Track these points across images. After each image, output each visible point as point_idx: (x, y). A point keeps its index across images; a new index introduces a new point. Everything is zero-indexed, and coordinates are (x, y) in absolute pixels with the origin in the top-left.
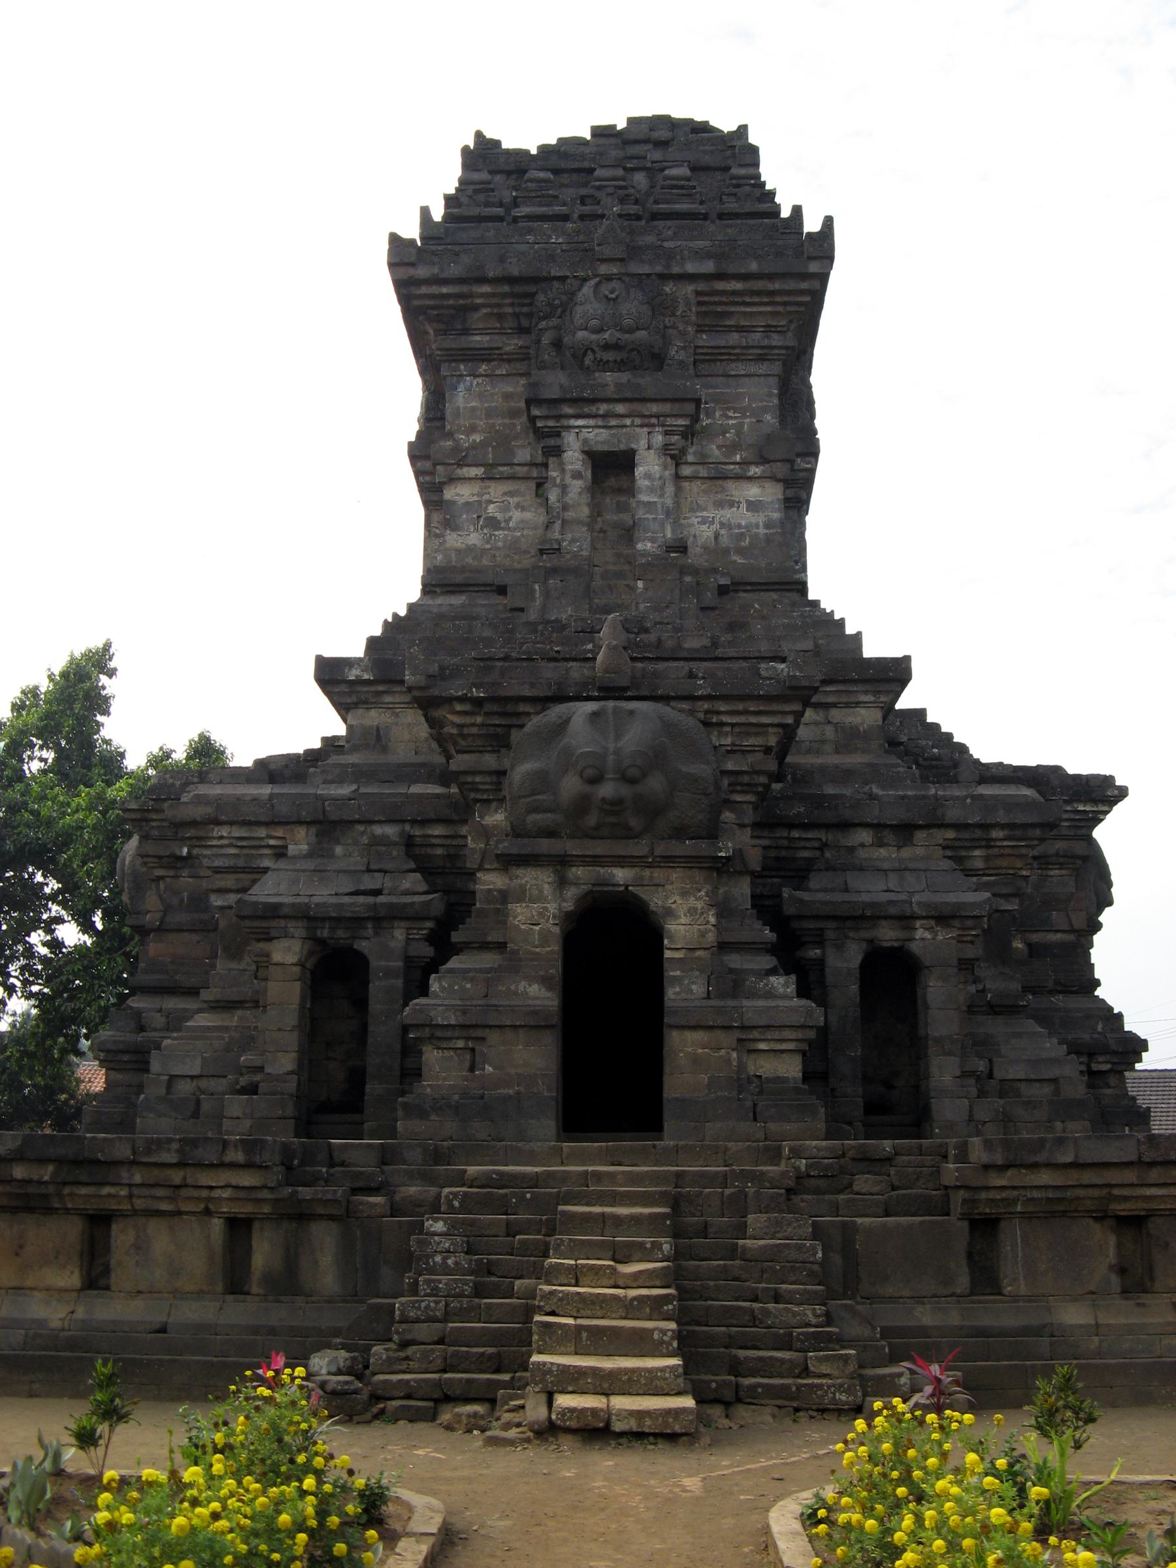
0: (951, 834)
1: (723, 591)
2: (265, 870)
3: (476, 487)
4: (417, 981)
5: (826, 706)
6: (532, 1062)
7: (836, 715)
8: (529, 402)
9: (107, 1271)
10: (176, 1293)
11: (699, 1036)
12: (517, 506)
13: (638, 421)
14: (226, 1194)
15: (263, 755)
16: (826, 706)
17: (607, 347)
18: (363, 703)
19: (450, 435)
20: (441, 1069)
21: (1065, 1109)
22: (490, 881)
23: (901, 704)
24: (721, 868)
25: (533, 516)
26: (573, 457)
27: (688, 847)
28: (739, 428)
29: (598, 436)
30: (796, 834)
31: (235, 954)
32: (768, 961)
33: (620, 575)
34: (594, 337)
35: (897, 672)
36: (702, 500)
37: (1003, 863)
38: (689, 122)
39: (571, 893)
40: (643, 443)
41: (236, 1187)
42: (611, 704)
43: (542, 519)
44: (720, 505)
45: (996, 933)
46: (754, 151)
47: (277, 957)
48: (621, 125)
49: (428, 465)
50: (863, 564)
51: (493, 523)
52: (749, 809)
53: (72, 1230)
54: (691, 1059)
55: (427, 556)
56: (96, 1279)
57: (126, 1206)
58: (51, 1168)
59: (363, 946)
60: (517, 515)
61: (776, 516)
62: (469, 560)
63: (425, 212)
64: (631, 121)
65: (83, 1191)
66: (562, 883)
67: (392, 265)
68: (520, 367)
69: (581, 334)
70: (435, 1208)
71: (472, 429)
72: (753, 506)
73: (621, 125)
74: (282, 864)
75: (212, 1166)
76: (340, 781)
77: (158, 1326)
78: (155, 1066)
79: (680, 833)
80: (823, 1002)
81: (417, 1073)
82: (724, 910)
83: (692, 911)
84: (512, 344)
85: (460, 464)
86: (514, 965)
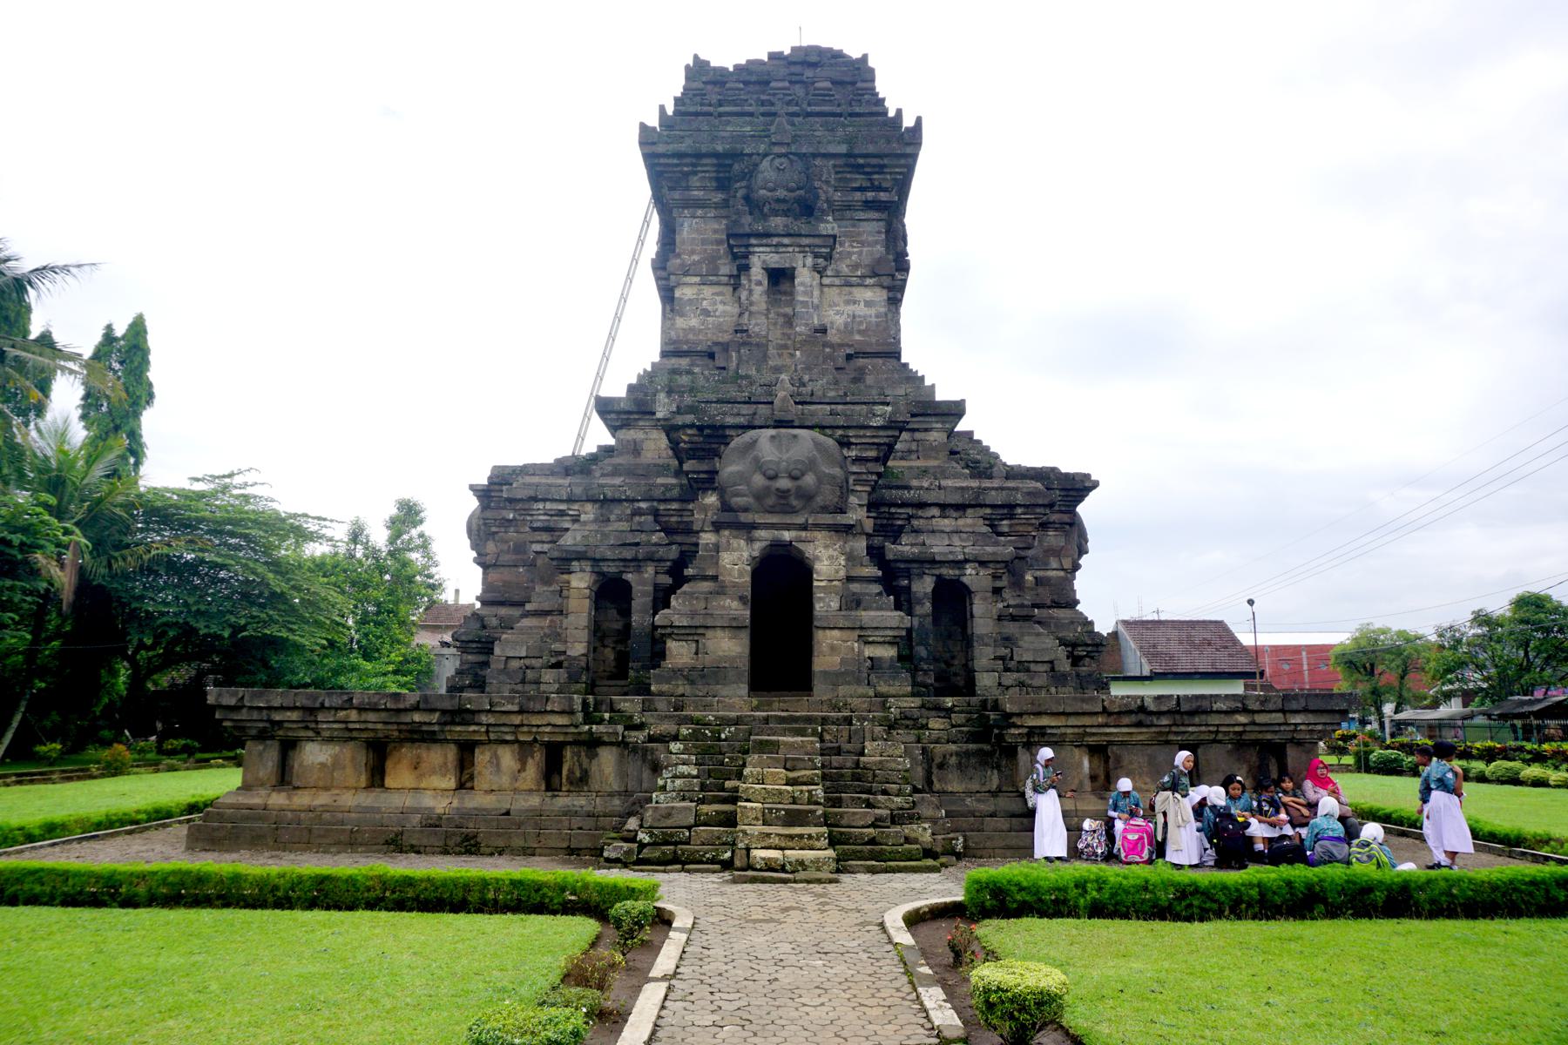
0: (988, 511)
1: (849, 357)
2: (567, 530)
3: (695, 290)
4: (662, 599)
5: (913, 430)
6: (730, 647)
7: (918, 435)
8: (729, 236)
9: (472, 778)
10: (515, 790)
11: (836, 633)
14: (548, 729)
15: (560, 456)
16: (913, 430)
17: (778, 201)
18: (626, 425)
19: (679, 256)
20: (679, 653)
21: (1058, 678)
22: (707, 538)
23: (959, 428)
24: (847, 530)
25: (733, 309)
26: (757, 272)
27: (827, 519)
28: (860, 254)
29: (774, 260)
30: (893, 510)
31: (548, 583)
32: (876, 588)
33: (785, 347)
35: (955, 410)
36: (836, 299)
37: (1020, 528)
38: (830, 50)
39: (758, 546)
40: (800, 263)
41: (554, 726)
42: (783, 431)
43: (736, 310)
44: (847, 302)
45: (1012, 568)
46: (872, 71)
47: (574, 584)
48: (787, 52)
49: (664, 274)
50: (937, 345)
51: (706, 313)
52: (865, 496)
53: (451, 753)
54: (831, 648)
55: (663, 332)
56: (465, 783)
57: (484, 738)
58: (437, 715)
59: (629, 577)
60: (721, 308)
61: (883, 310)
62: (691, 336)
63: (662, 109)
64: (793, 49)
65: (458, 728)
66: (751, 540)
67: (642, 144)
68: (723, 212)
69: (762, 192)
70: (676, 738)
71: (693, 252)
72: (868, 304)
73: (787, 52)
74: (576, 526)
75: (539, 712)
76: (613, 474)
78: (497, 651)
79: (825, 509)
80: (910, 613)
81: (662, 655)
82: (851, 558)
83: (831, 557)
84: (718, 197)
85: (686, 274)
86: (721, 591)
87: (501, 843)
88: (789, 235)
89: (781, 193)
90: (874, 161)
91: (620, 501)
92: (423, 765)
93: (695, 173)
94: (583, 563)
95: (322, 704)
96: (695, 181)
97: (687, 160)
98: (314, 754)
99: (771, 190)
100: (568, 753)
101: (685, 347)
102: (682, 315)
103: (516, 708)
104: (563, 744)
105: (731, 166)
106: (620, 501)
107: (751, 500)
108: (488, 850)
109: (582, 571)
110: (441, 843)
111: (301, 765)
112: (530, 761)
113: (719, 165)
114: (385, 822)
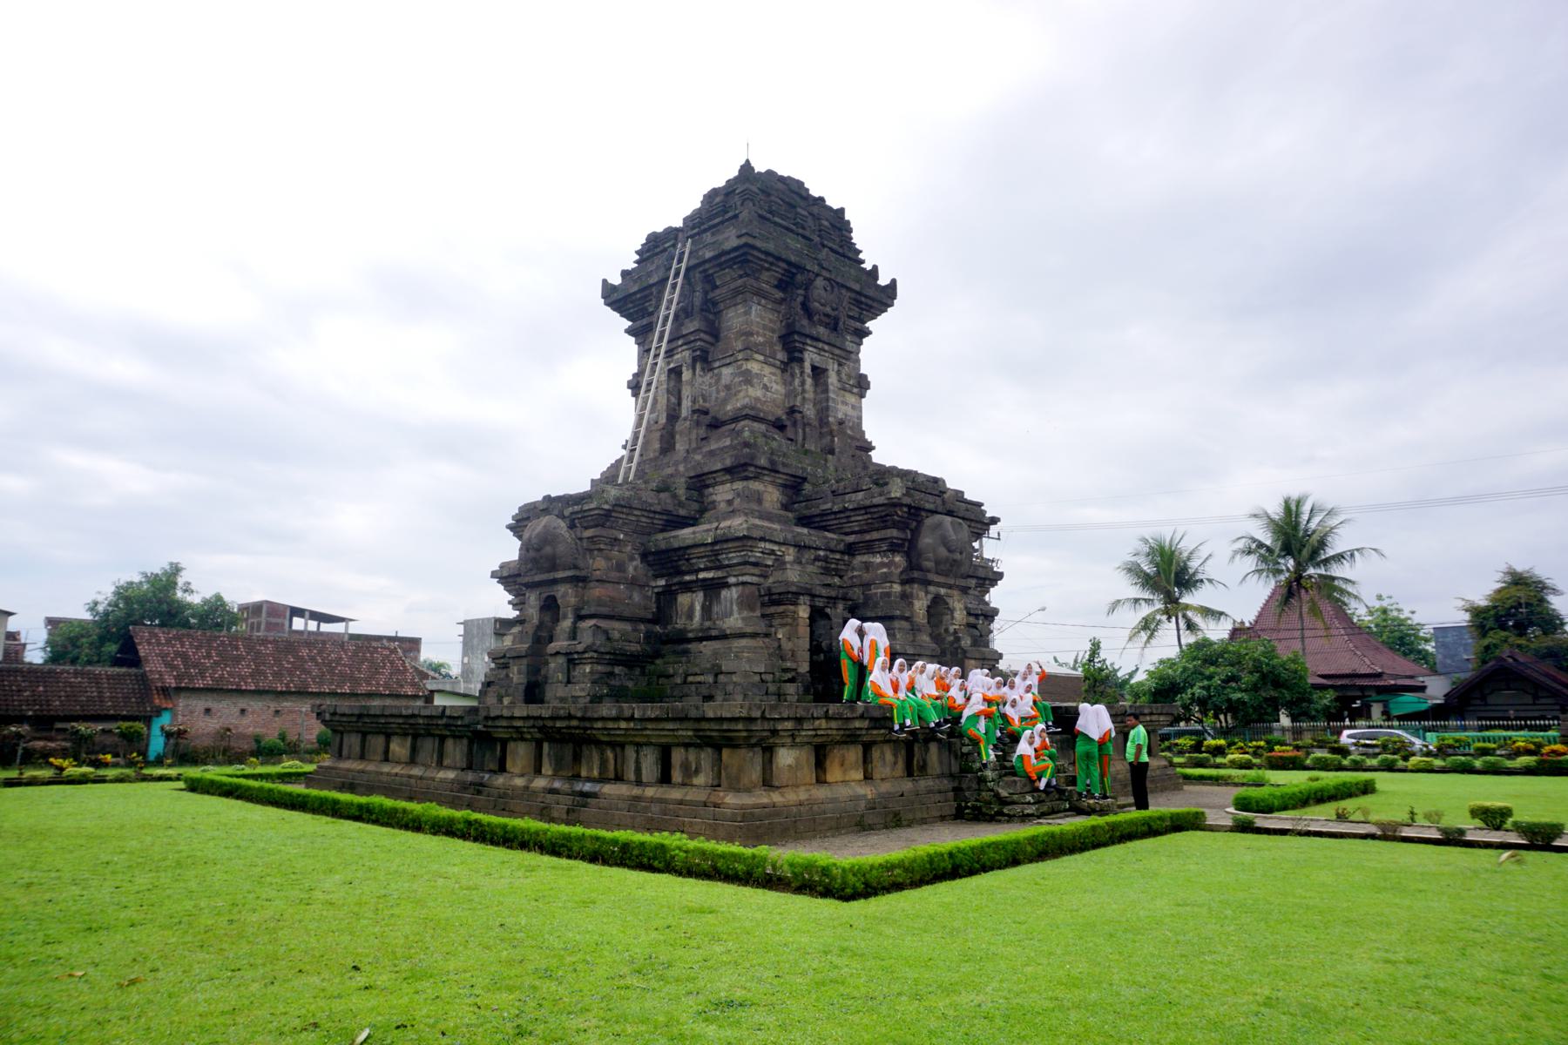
29: (817, 358)
51: (765, 387)
56: (868, 777)
60: (775, 386)
66: (927, 593)
84: (779, 295)
87: (910, 816)
89: (828, 310)
91: (810, 548)
93: (768, 270)
96: (765, 276)
98: (786, 757)
106: (810, 548)
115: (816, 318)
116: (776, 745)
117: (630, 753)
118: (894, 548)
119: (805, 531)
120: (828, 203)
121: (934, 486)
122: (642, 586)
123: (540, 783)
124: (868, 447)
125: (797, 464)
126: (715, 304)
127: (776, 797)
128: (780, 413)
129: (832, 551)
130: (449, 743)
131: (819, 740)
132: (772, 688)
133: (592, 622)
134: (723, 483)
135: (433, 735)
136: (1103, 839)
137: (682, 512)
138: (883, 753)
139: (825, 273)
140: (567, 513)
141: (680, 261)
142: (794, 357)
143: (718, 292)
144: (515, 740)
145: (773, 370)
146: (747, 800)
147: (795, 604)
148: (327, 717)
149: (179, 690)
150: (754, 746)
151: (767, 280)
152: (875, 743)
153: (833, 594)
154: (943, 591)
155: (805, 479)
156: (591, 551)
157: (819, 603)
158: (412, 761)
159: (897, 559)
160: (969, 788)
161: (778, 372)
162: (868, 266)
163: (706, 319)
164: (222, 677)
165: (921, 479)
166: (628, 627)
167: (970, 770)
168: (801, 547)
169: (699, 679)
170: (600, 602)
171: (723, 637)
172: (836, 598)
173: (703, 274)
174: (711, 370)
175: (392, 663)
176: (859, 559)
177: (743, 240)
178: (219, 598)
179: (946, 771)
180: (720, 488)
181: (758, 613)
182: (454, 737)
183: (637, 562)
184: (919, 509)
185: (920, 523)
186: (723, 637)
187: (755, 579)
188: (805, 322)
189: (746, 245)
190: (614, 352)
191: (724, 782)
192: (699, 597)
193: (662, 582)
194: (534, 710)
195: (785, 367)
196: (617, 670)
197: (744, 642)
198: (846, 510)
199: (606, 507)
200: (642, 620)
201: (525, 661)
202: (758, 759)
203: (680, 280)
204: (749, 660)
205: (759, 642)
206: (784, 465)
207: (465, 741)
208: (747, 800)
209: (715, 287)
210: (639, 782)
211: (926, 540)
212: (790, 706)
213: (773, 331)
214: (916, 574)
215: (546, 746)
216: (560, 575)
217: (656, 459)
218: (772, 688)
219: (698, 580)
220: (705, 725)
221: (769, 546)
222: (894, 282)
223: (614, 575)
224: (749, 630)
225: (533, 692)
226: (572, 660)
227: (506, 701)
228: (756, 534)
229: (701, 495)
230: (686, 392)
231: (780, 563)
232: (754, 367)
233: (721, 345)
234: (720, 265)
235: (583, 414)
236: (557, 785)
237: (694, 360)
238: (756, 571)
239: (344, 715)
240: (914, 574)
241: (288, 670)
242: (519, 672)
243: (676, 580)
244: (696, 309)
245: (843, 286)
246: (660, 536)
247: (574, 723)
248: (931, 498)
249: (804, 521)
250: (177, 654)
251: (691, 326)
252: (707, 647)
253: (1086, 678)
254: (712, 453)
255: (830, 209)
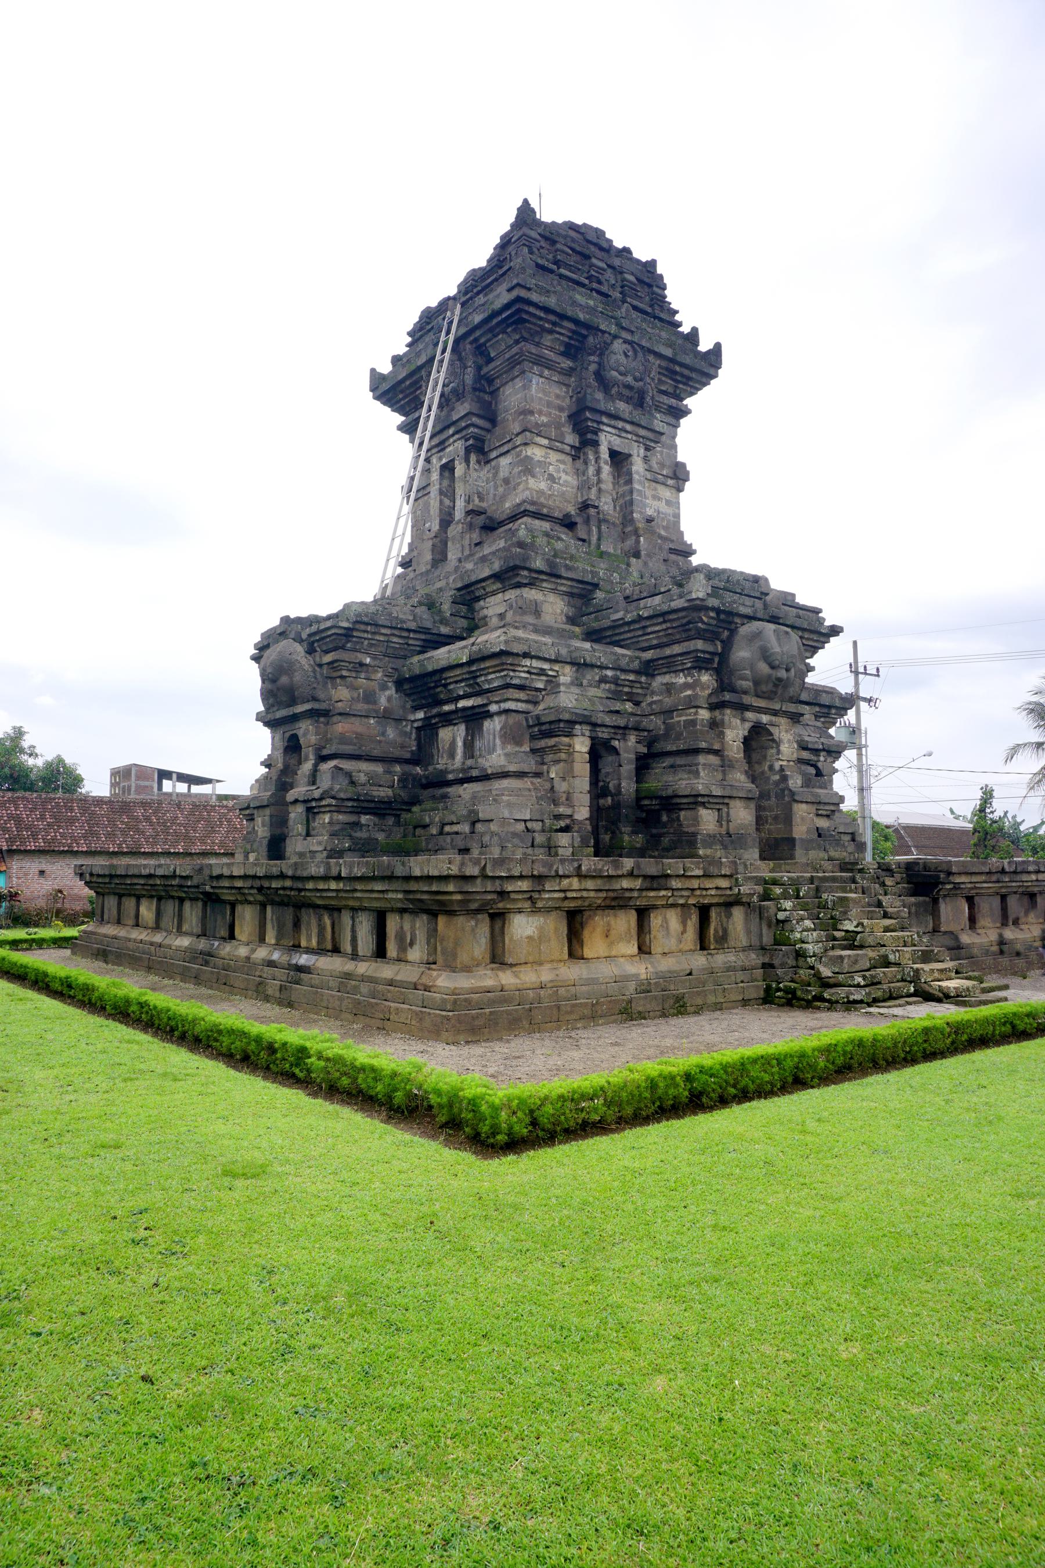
12: (564, 471)
13: (634, 438)
29: (618, 444)
34: (620, 377)
47: (578, 748)
51: (551, 478)
53: (633, 916)
56: (644, 950)
58: (640, 880)
60: (564, 477)
66: (743, 720)
77: (688, 972)
84: (567, 363)
87: (700, 1001)
88: (632, 423)
89: (629, 379)
90: (686, 372)
91: (593, 666)
92: (613, 932)
93: (551, 332)
94: (585, 727)
95: (557, 871)
96: (547, 340)
97: (552, 318)
98: (523, 927)
99: (621, 374)
100: (713, 913)
101: (545, 511)
102: (533, 476)
103: (700, 873)
104: (711, 905)
105: (585, 337)
106: (593, 666)
107: (751, 684)
108: (692, 1009)
109: (583, 735)
110: (660, 1008)
111: (511, 940)
112: (689, 923)
113: (573, 332)
114: (610, 993)
115: (614, 391)
116: (509, 911)
117: (346, 918)
118: (701, 664)
119: (587, 645)
120: (636, 255)
121: (756, 586)
122: (398, 720)
123: (261, 953)
124: (687, 552)
125: (583, 568)
126: (490, 381)
127: (507, 978)
128: (572, 510)
129: (623, 671)
130: (187, 905)
131: (572, 904)
132: (539, 839)
133: (332, 763)
134: (494, 593)
135: (173, 897)
136: (940, 1045)
137: (444, 630)
138: (665, 920)
139: (625, 335)
140: (304, 636)
141: (448, 333)
142: (586, 440)
143: (492, 365)
144: (241, 903)
145: (562, 457)
146: (464, 982)
147: (570, 735)
148: (88, 878)
149: (11, 852)
150: (478, 911)
151: (549, 346)
152: (655, 907)
153: (622, 722)
154: (765, 719)
155: (596, 586)
156: (333, 678)
157: (603, 734)
158: (157, 927)
159: (705, 678)
160: (783, 965)
161: (569, 459)
162: (685, 329)
163: (480, 400)
164: (54, 839)
165: (736, 578)
166: (378, 768)
167: (787, 942)
168: (580, 665)
169: (455, 828)
170: (343, 739)
171: (485, 777)
172: (625, 728)
173: (474, 344)
174: (488, 462)
175: (229, 821)
176: (660, 680)
177: (515, 293)
178: (60, 760)
179: (755, 941)
180: (491, 600)
181: (526, 748)
182: (191, 899)
183: (391, 691)
184: (730, 614)
185: (733, 632)
186: (485, 777)
187: (521, 706)
188: (599, 396)
189: (519, 299)
190: (387, 454)
191: (440, 959)
192: (461, 730)
193: (420, 715)
194: (276, 867)
195: (577, 453)
196: (364, 819)
197: (505, 783)
198: (640, 618)
199: (345, 624)
200: (398, 760)
201: (267, 811)
202: (483, 929)
203: (447, 355)
204: (509, 805)
205: (527, 783)
206: (568, 568)
207: (200, 904)
208: (464, 982)
209: (490, 360)
210: (355, 956)
211: (741, 653)
212: (562, 861)
213: (561, 409)
214: (727, 696)
215: (269, 909)
216: (300, 709)
217: (428, 572)
218: (539, 839)
219: (456, 711)
220: (413, 886)
221: (536, 663)
222: (718, 347)
223: (361, 707)
224: (512, 768)
225: (276, 847)
226: (311, 812)
227: (252, 857)
228: (517, 648)
229: (471, 610)
230: (460, 490)
231: (553, 684)
232: (536, 453)
233: (498, 430)
234: (491, 330)
235: (345, 522)
236: (276, 956)
237: (468, 450)
238: (522, 695)
239: (99, 876)
240: (726, 698)
241: (122, 831)
242: (263, 825)
243: (435, 711)
244: (468, 388)
245: (651, 351)
246: (415, 659)
247: (288, 883)
248: (748, 601)
249: (593, 636)
250: (11, 817)
251: (462, 409)
252: (467, 791)
253: (975, 831)
254: (484, 559)
255: (638, 261)
